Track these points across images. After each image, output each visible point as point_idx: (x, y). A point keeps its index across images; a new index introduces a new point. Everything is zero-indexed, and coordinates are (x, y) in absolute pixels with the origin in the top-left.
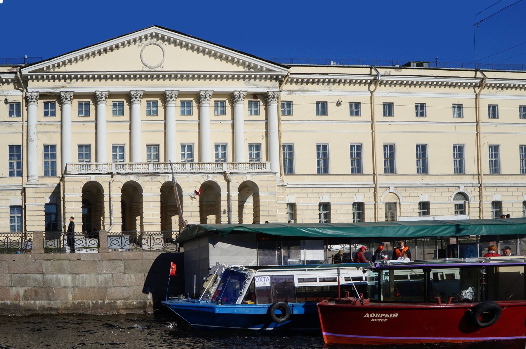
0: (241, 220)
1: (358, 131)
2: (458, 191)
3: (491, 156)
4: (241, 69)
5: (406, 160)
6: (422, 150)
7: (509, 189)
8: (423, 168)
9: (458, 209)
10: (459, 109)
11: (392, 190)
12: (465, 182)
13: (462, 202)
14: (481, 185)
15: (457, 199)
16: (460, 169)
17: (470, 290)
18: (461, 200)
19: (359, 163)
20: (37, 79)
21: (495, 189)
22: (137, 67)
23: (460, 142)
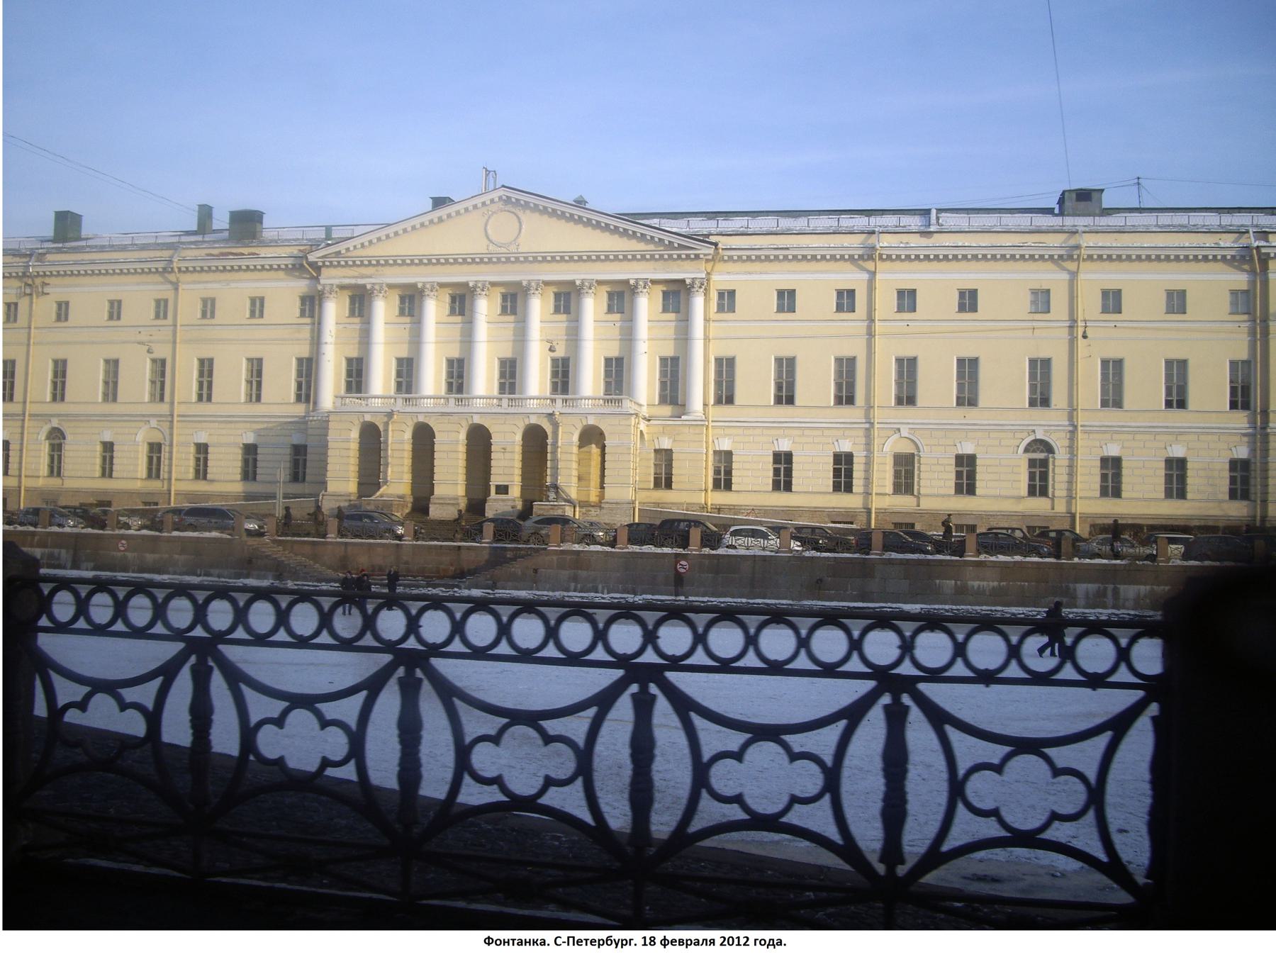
0: (55, 467)
1: (784, 336)
2: (1032, 438)
3: (107, 372)
4: (641, 246)
5: (938, 384)
6: (968, 369)
7: (1138, 437)
8: (968, 397)
9: (1107, 468)
10: (1042, 300)
11: (905, 433)
12: (1049, 424)
13: (1041, 456)
14: (1076, 427)
15: (1034, 451)
16: (1041, 399)
17: (46, 593)
18: (1042, 451)
19: (851, 386)
20: (331, 265)
21: (1108, 436)
22: (477, 246)
23: (1043, 355)
